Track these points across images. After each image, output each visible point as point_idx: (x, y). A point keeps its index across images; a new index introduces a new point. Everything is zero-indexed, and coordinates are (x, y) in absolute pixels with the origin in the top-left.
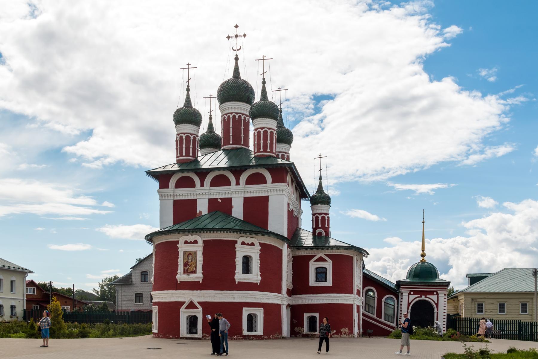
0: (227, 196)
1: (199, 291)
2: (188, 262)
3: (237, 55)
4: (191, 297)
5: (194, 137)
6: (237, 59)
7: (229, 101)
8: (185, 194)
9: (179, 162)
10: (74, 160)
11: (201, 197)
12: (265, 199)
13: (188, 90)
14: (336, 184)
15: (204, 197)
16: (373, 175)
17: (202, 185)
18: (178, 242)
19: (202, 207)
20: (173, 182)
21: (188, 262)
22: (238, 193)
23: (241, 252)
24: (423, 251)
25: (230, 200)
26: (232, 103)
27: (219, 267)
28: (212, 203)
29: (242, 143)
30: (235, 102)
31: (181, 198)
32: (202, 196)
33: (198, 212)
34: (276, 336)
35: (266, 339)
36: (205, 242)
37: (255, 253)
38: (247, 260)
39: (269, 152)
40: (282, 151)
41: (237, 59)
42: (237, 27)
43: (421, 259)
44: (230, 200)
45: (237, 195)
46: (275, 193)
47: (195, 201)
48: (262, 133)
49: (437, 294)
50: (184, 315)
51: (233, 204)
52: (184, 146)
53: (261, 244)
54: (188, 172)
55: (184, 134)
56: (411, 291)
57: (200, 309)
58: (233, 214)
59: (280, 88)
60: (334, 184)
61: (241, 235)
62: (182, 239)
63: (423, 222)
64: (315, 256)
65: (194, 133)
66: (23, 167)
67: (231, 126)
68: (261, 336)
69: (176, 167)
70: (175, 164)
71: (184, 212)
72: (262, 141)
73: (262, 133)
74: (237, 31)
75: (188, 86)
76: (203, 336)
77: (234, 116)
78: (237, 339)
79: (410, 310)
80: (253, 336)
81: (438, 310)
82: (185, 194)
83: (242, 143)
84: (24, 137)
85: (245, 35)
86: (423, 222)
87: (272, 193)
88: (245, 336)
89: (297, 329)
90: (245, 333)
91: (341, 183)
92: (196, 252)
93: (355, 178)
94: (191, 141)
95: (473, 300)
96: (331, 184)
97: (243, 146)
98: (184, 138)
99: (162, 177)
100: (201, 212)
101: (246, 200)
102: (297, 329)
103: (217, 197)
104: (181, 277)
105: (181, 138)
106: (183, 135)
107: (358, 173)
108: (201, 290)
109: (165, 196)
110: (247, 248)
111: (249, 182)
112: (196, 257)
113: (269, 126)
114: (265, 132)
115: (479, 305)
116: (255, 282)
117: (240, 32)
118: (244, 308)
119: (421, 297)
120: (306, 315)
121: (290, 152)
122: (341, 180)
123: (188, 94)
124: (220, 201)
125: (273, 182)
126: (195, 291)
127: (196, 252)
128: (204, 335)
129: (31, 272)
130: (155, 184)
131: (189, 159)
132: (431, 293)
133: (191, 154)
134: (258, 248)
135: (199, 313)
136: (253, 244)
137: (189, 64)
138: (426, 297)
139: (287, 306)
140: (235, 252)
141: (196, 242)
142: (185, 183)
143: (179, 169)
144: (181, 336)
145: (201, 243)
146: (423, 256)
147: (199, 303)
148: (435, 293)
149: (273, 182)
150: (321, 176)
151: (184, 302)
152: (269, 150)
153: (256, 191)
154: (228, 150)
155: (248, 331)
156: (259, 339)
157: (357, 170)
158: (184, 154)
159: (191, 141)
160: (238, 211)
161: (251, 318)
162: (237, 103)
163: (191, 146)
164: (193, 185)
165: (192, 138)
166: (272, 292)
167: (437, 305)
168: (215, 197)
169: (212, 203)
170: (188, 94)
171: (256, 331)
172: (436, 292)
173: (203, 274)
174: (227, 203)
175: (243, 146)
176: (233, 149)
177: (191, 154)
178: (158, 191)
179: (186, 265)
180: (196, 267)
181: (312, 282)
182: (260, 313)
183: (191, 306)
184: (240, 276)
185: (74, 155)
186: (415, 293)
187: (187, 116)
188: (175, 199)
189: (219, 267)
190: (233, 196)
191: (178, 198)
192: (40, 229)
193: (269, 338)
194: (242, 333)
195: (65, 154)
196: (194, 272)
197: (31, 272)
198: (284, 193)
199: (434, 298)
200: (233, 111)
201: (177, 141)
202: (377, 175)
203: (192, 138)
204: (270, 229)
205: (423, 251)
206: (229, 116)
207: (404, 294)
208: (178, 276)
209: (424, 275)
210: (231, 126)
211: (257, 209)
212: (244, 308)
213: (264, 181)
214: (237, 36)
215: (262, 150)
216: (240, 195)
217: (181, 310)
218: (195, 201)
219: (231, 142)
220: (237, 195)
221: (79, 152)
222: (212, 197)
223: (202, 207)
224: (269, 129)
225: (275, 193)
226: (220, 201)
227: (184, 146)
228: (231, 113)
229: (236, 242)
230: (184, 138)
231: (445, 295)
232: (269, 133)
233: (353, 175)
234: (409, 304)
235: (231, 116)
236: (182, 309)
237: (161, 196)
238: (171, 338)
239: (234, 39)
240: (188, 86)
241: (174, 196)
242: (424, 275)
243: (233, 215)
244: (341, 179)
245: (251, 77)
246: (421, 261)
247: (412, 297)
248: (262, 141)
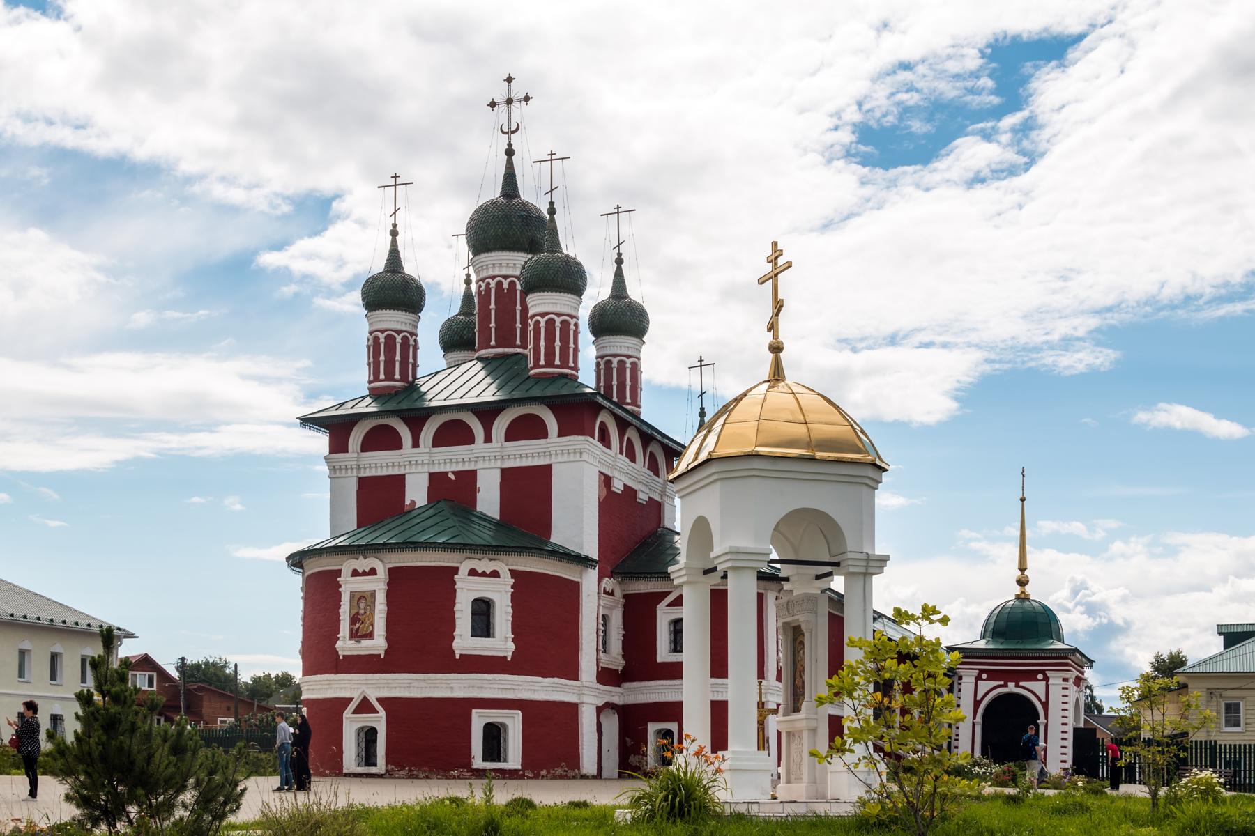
0: (467, 467)
1: (378, 676)
2: (358, 613)
3: (510, 145)
4: (364, 688)
5: (405, 339)
6: (510, 152)
7: (488, 250)
8: (381, 463)
9: (376, 394)
10: (289, 290)
11: (413, 469)
12: (546, 471)
13: (394, 233)
14: (1098, 330)
15: (420, 469)
16: (1219, 300)
17: (416, 444)
18: (338, 573)
19: (417, 493)
20: (356, 437)
21: (358, 613)
22: (489, 461)
23: (466, 592)
24: (1022, 570)
25: (473, 473)
26: (493, 254)
27: (420, 626)
28: (508, 475)
29: (518, 342)
30: (500, 253)
31: (373, 473)
32: (416, 465)
33: (407, 502)
34: (559, 771)
35: (529, 778)
36: (392, 572)
37: (501, 595)
38: (483, 610)
39: (557, 367)
40: (619, 352)
41: (510, 152)
42: (509, 80)
43: (1017, 590)
44: (473, 473)
45: (487, 465)
46: (565, 458)
47: (400, 479)
48: (542, 324)
49: (1046, 679)
50: (351, 725)
51: (480, 483)
52: (382, 358)
53: (514, 573)
54: (397, 409)
55: (383, 331)
56: (981, 671)
57: (382, 713)
58: (481, 507)
59: (618, 207)
60: (1090, 332)
61: (468, 555)
62: (347, 565)
63: (1023, 500)
64: (668, 593)
65: (403, 328)
66: (143, 318)
67: (493, 306)
68: (516, 771)
69: (362, 408)
70: (364, 397)
71: (378, 499)
72: (542, 343)
73: (542, 324)
74: (510, 90)
75: (395, 225)
76: (387, 771)
77: (499, 284)
78: (459, 778)
79: (979, 718)
80: (494, 770)
81: (1046, 718)
82: (381, 463)
83: (518, 342)
84: (149, 232)
85: (527, 99)
86: (1023, 500)
87: (560, 459)
88: (477, 770)
89: (633, 760)
90: (478, 762)
91: (1112, 328)
92: (373, 593)
93: (1161, 309)
94: (398, 346)
95: (1211, 693)
96: (1081, 333)
97: (519, 350)
98: (382, 340)
99: (338, 428)
100: (413, 502)
101: (504, 472)
102: (633, 760)
103: (448, 468)
104: (345, 646)
105: (376, 339)
106: (379, 334)
107: (1167, 293)
108: (383, 672)
109: (340, 469)
110: (484, 582)
111: (439, 441)
112: (374, 603)
113: (558, 309)
114: (551, 323)
115: (1229, 707)
116: (502, 654)
117: (518, 93)
118: (474, 711)
119: (1006, 685)
120: (652, 728)
121: (643, 355)
122: (1113, 319)
123: (510, 165)
124: (452, 477)
125: (561, 434)
126: (370, 676)
127: (373, 593)
128: (390, 767)
129: (131, 636)
130: (320, 441)
131: (394, 387)
132: (1031, 676)
133: (397, 376)
134: (507, 582)
135: (379, 721)
136: (495, 574)
137: (396, 177)
138: (1018, 686)
139: (599, 710)
140: (455, 591)
141: (373, 572)
142: (381, 439)
143: (375, 410)
144: (345, 771)
145: (382, 573)
146: (1022, 582)
147: (380, 700)
148: (1040, 676)
149: (561, 434)
150: (702, 409)
151: (352, 699)
152: (557, 362)
153: (526, 454)
154: (487, 358)
155: (485, 760)
156: (510, 778)
157: (1162, 285)
158: (382, 376)
159: (398, 346)
160: (489, 500)
161: (494, 735)
162: (505, 253)
163: (398, 358)
164: (396, 444)
165: (399, 339)
166: (544, 676)
167: (1045, 705)
168: (442, 469)
169: (437, 480)
170: (510, 165)
171: (505, 761)
172: (1043, 672)
173: (387, 638)
174: (468, 479)
175: (519, 350)
176: (497, 357)
177: (397, 376)
178: (325, 458)
179: (354, 619)
180: (373, 625)
181: (345, 646)
182: (513, 723)
183: (365, 706)
184: (464, 642)
185: (284, 275)
186: (993, 675)
187: (393, 291)
188: (362, 475)
189: (420, 626)
190: (479, 466)
191: (368, 473)
192: (196, 499)
193: (537, 776)
194: (470, 763)
195: (262, 271)
196: (370, 636)
197: (131, 636)
198: (585, 457)
199: (1038, 687)
200: (497, 273)
201: (368, 347)
202: (1231, 298)
203: (399, 339)
204: (558, 537)
205: (1022, 570)
206: (488, 284)
207: (964, 680)
208: (339, 645)
209: (1024, 633)
210: (493, 306)
211: (529, 492)
212: (474, 711)
213: (542, 433)
214: (510, 101)
215: (542, 362)
216: (493, 464)
217: (345, 715)
218: (400, 479)
219: (493, 343)
220: (487, 465)
221: (299, 266)
222: (436, 469)
223: (417, 493)
224: (559, 315)
225: (565, 458)
226: (452, 477)
227: (382, 358)
228: (493, 277)
229: (455, 570)
230: (382, 340)
231: (1065, 680)
232: (558, 324)
233: (1146, 304)
234: (977, 704)
235: (493, 284)
236: (348, 714)
237: (333, 469)
238: (326, 776)
239: (514, 96)
240: (395, 225)
241: (359, 468)
242: (1024, 633)
243: (479, 508)
244: (1109, 315)
245: (531, 193)
246: (1018, 597)
247: (984, 686)
248: (542, 343)
